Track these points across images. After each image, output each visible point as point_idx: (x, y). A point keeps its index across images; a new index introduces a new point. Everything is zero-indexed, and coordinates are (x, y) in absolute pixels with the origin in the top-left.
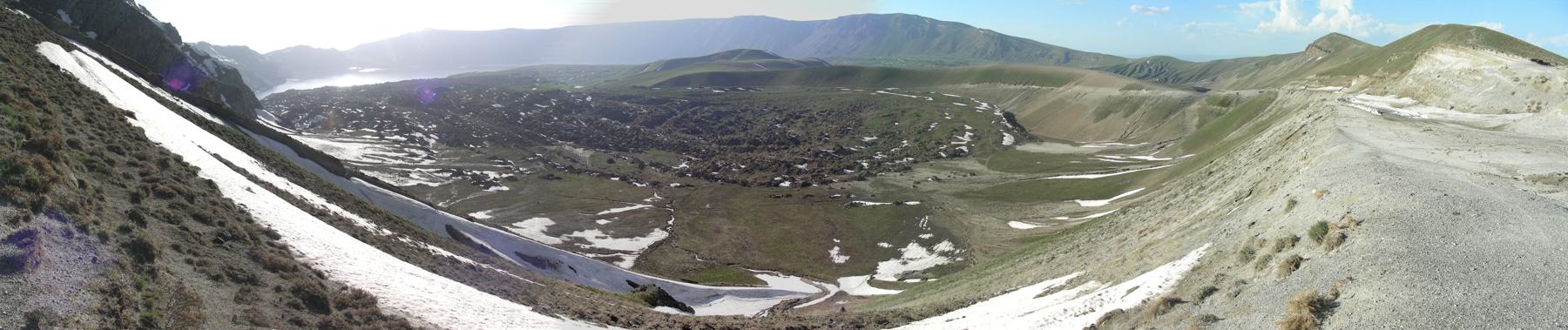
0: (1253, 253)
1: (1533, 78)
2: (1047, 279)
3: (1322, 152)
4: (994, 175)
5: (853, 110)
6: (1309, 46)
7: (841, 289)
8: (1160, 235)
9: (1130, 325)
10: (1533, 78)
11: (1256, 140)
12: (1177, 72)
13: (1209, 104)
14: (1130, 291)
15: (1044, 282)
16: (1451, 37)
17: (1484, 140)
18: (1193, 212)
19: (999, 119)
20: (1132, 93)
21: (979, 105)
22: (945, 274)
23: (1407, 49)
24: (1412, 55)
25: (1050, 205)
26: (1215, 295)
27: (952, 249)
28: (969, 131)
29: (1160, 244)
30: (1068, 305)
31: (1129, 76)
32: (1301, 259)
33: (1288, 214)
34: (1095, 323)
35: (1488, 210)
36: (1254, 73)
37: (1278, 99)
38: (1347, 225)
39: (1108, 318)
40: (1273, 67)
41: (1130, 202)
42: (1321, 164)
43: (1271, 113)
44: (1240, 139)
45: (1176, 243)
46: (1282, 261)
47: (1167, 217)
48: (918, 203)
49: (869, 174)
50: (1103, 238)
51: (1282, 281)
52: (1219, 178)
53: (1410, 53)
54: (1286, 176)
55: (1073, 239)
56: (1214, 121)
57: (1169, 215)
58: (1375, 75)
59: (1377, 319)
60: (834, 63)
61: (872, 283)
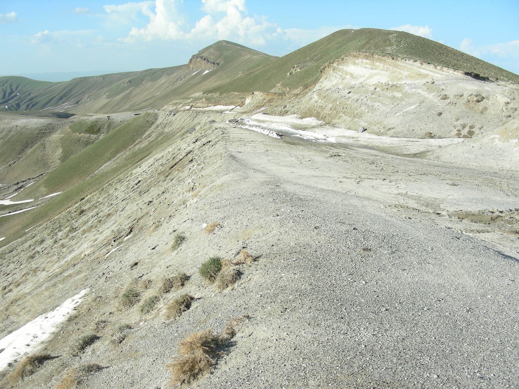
0: (137, 295)
1: (466, 96)
3: (213, 181)
6: (193, 57)
8: (26, 288)
10: (466, 96)
11: (134, 171)
12: (32, 95)
13: (74, 131)
16: (365, 45)
17: (402, 168)
18: (64, 258)
23: (312, 59)
24: (318, 67)
26: (97, 344)
32: (192, 299)
33: (176, 252)
35: (404, 246)
36: (128, 91)
37: (159, 122)
38: (243, 261)
40: (149, 84)
42: (211, 195)
43: (151, 139)
44: (115, 171)
45: (47, 293)
46: (171, 302)
47: (34, 266)
51: (172, 323)
52: (92, 217)
53: (315, 64)
54: (171, 210)
57: (35, 264)
58: (273, 91)
59: (277, 358)
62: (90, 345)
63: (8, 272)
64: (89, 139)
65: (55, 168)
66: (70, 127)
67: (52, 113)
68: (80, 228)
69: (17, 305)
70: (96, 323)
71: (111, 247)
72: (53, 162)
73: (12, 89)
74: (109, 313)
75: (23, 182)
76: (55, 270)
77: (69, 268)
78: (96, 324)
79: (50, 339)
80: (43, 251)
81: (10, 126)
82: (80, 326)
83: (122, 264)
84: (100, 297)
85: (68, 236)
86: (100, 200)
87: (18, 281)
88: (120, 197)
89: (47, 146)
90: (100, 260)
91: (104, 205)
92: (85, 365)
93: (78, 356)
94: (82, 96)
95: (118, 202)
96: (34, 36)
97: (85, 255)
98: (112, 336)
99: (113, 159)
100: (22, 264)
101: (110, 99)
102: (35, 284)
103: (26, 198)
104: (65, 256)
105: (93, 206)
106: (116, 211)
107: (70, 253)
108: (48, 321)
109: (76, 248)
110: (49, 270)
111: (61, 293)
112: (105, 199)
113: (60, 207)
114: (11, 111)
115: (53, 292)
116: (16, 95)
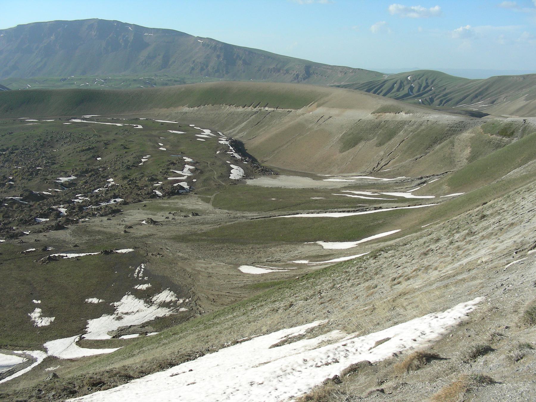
2: (284, 328)
4: (221, 214)
5: (43, 146)
7: (50, 353)
8: (416, 284)
9: (378, 378)
12: (447, 91)
13: (485, 132)
14: (379, 343)
15: (281, 331)
18: (459, 260)
19: (225, 149)
20: (388, 116)
21: (200, 132)
22: (167, 327)
25: (288, 247)
26: (490, 356)
27: (174, 299)
28: (188, 163)
29: (416, 294)
30: (308, 355)
31: (385, 95)
34: (338, 374)
39: (354, 369)
41: (382, 245)
47: (426, 264)
48: (131, 250)
49: (68, 221)
50: (349, 284)
52: (494, 223)
55: (314, 284)
56: (493, 153)
60: (14, 87)
61: (81, 343)
62: (483, 355)
63: (399, 265)
64: (501, 141)
65: (461, 168)
66: (482, 127)
67: (465, 110)
68: (479, 233)
69: (404, 298)
70: (492, 334)
71: (512, 258)
72: (460, 161)
73: (427, 83)
74: (505, 327)
75: (427, 177)
76: (447, 271)
77: (464, 272)
78: (491, 336)
79: (437, 339)
80: (437, 250)
81: (421, 120)
82: (472, 333)
83: (524, 279)
84: (497, 308)
85: (465, 239)
86: (504, 207)
87: (408, 275)
88: (527, 207)
89: (456, 144)
90: (498, 269)
91: (508, 213)
92: (477, 375)
93: (468, 363)
94: (499, 96)
95: (524, 212)
96: (455, 30)
97: (482, 262)
98: (510, 351)
99: (523, 166)
100: (414, 259)
101: (528, 101)
102: (425, 281)
103: (427, 194)
104: (460, 259)
105: (496, 212)
106: (520, 222)
107: (465, 256)
108: (438, 321)
109: (473, 253)
110: (441, 269)
111: (453, 295)
112: (510, 206)
113: (461, 208)
114: (423, 105)
115: (444, 292)
116: (431, 90)
